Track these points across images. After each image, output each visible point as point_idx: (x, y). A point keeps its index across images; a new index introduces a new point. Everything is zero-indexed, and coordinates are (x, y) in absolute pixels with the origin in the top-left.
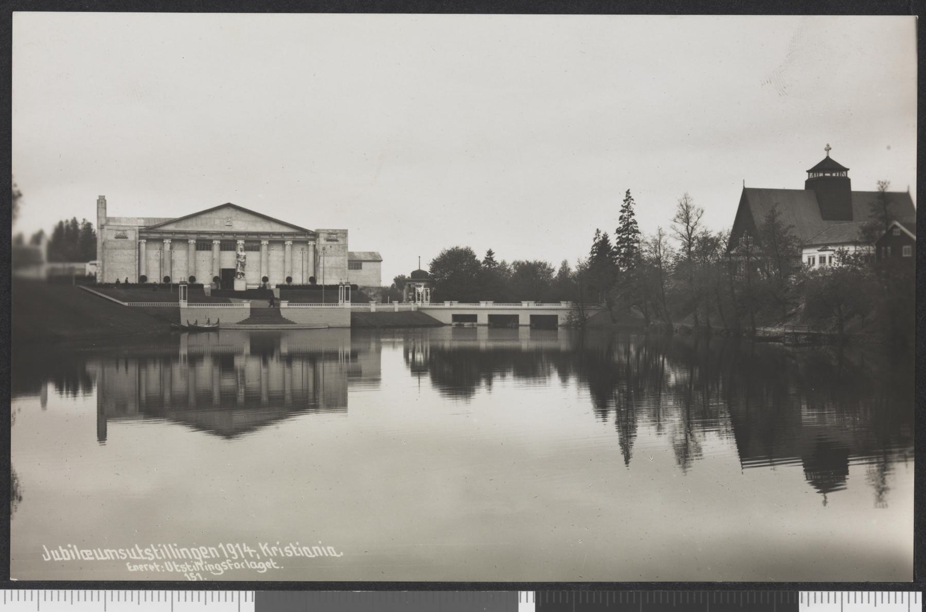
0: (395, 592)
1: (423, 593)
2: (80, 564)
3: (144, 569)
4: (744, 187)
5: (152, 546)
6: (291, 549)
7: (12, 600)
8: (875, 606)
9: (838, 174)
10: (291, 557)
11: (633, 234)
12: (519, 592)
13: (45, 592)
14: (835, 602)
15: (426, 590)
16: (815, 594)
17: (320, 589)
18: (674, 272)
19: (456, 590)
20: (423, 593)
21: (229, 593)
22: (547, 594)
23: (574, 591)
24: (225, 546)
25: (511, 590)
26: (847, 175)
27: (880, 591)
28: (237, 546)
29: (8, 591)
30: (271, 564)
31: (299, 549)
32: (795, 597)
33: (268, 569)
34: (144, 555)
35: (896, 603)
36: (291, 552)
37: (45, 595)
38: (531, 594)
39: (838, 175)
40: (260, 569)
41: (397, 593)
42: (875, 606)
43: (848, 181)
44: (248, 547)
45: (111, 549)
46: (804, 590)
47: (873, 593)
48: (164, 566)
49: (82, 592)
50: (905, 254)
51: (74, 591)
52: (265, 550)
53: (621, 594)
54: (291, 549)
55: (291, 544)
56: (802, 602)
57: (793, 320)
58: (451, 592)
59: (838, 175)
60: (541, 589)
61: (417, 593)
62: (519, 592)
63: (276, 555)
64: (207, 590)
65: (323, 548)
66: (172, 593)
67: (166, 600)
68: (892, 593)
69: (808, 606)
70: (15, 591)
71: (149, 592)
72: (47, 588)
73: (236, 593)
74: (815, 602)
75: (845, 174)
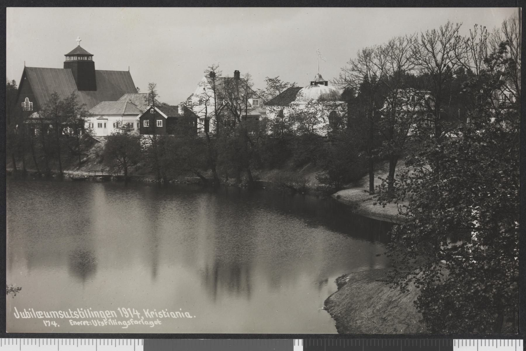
1: (239, 340)
2: (36, 320)
4: (25, 66)
5: (78, 309)
6: (162, 313)
7: (81, 345)
8: (497, 347)
9: (81, 58)
10: (30, 318)
11: (407, 93)
15: (241, 338)
16: (462, 340)
17: (181, 338)
18: (126, 128)
20: (239, 340)
21: (129, 340)
22: (310, 340)
24: (121, 309)
25: (290, 338)
26: (92, 59)
27: (95, 338)
28: (129, 309)
29: (3, 339)
30: (158, 322)
31: (167, 313)
32: (451, 342)
34: (74, 315)
35: (9, 344)
36: (162, 315)
37: (24, 341)
38: (301, 341)
39: (82, 59)
40: (123, 326)
41: (224, 340)
42: (497, 347)
43: (92, 63)
44: (136, 311)
45: (54, 311)
47: (507, 340)
49: (45, 340)
50: (161, 122)
51: (25, 339)
52: (147, 314)
53: (371, 341)
54: (162, 313)
55: (163, 311)
56: (455, 346)
57: (86, 165)
59: (82, 59)
60: (304, 337)
61: (235, 340)
63: (153, 317)
65: (182, 313)
66: (97, 340)
67: (131, 345)
68: (506, 340)
69: (459, 347)
71: (83, 340)
72: (116, 338)
73: (133, 340)
75: (91, 58)
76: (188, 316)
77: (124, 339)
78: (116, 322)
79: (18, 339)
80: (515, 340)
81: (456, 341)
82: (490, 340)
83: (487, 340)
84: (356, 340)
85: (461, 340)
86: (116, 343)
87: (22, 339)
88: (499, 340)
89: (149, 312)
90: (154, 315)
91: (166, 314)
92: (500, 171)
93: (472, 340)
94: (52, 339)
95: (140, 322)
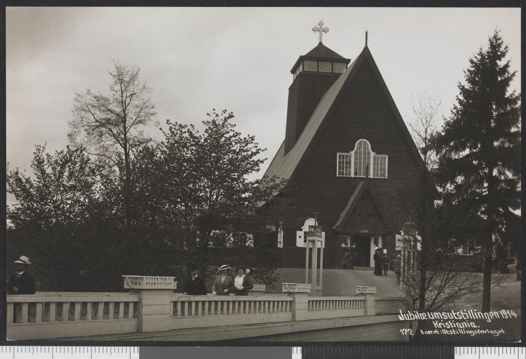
0: (170, 347)
3: (430, 333)
6: (449, 324)
12: (292, 347)
13: (18, 347)
14: (475, 353)
16: (464, 348)
17: (177, 346)
19: (255, 346)
23: (324, 347)
25: (288, 346)
27: (502, 347)
31: (454, 324)
33: (475, 334)
35: (2, 352)
37: (18, 349)
38: (299, 349)
46: (458, 346)
48: (442, 331)
52: (436, 325)
56: (456, 353)
58: (253, 347)
62: (292, 347)
64: (112, 346)
66: (95, 348)
68: (509, 348)
69: (460, 355)
70: (8, 347)
74: (464, 353)
76: (473, 326)
77: (119, 347)
78: (464, 331)
79: (12, 347)
80: (502, 347)
81: (457, 349)
82: (515, 348)
83: (489, 348)
84: (355, 348)
85: (462, 348)
86: (111, 351)
87: (16, 347)
88: (501, 348)
89: (438, 323)
90: (442, 326)
91: (453, 325)
92: (245, 199)
93: (474, 348)
94: (46, 347)
95: (486, 331)
